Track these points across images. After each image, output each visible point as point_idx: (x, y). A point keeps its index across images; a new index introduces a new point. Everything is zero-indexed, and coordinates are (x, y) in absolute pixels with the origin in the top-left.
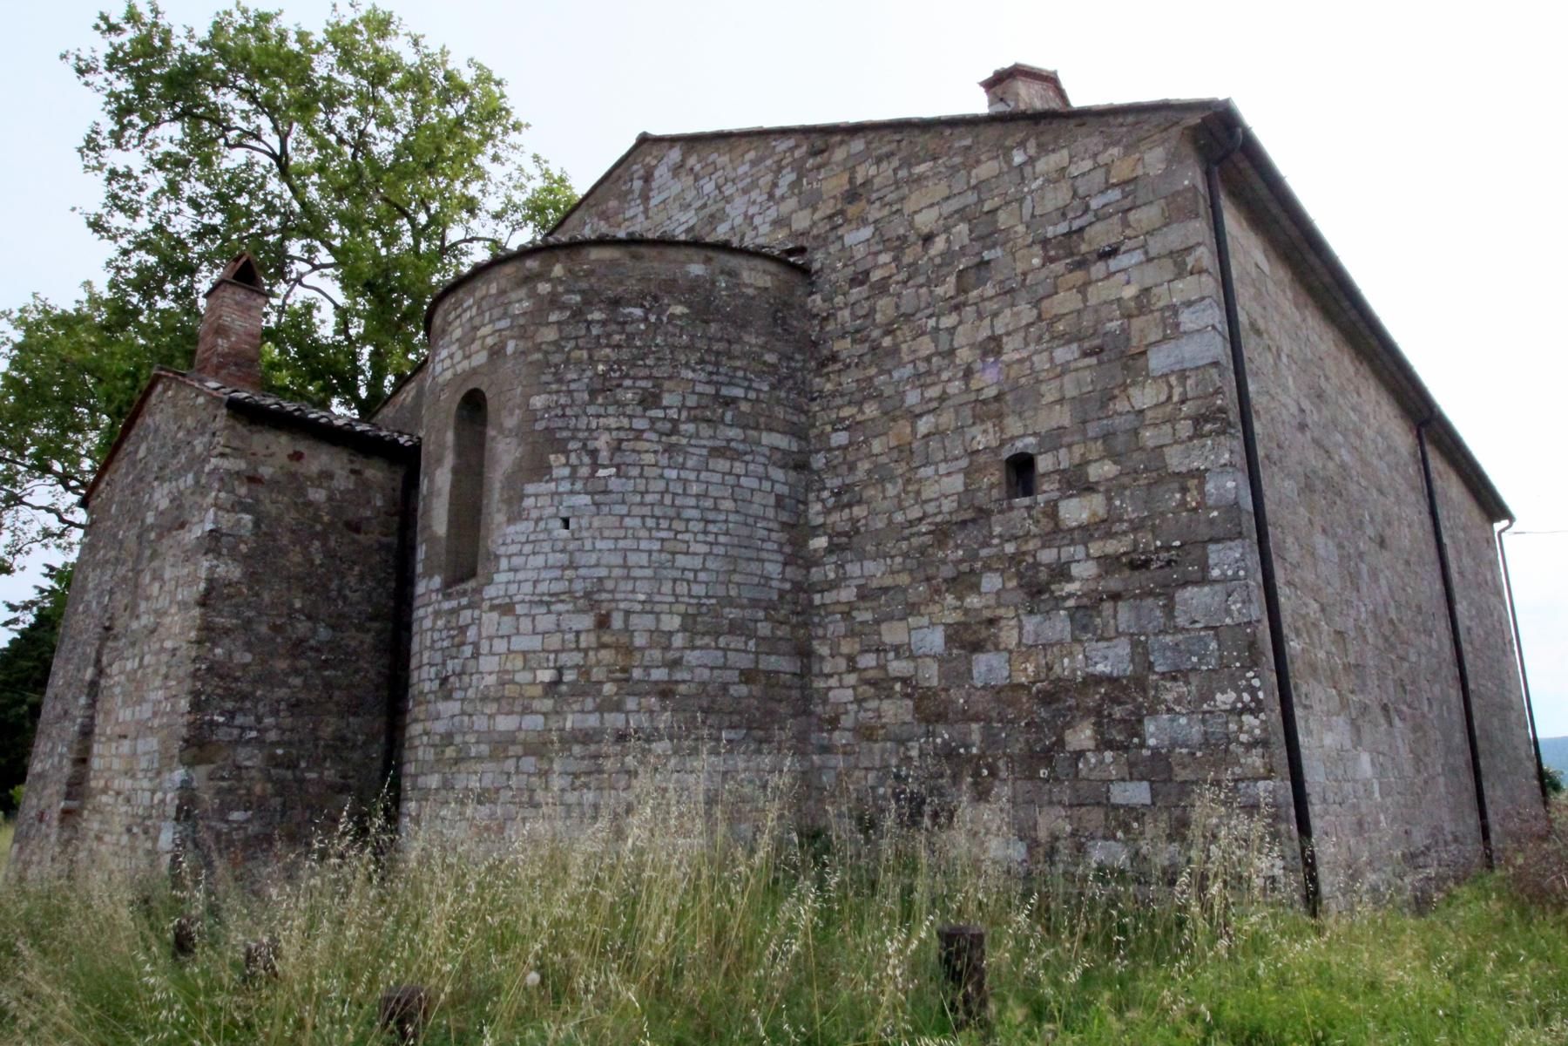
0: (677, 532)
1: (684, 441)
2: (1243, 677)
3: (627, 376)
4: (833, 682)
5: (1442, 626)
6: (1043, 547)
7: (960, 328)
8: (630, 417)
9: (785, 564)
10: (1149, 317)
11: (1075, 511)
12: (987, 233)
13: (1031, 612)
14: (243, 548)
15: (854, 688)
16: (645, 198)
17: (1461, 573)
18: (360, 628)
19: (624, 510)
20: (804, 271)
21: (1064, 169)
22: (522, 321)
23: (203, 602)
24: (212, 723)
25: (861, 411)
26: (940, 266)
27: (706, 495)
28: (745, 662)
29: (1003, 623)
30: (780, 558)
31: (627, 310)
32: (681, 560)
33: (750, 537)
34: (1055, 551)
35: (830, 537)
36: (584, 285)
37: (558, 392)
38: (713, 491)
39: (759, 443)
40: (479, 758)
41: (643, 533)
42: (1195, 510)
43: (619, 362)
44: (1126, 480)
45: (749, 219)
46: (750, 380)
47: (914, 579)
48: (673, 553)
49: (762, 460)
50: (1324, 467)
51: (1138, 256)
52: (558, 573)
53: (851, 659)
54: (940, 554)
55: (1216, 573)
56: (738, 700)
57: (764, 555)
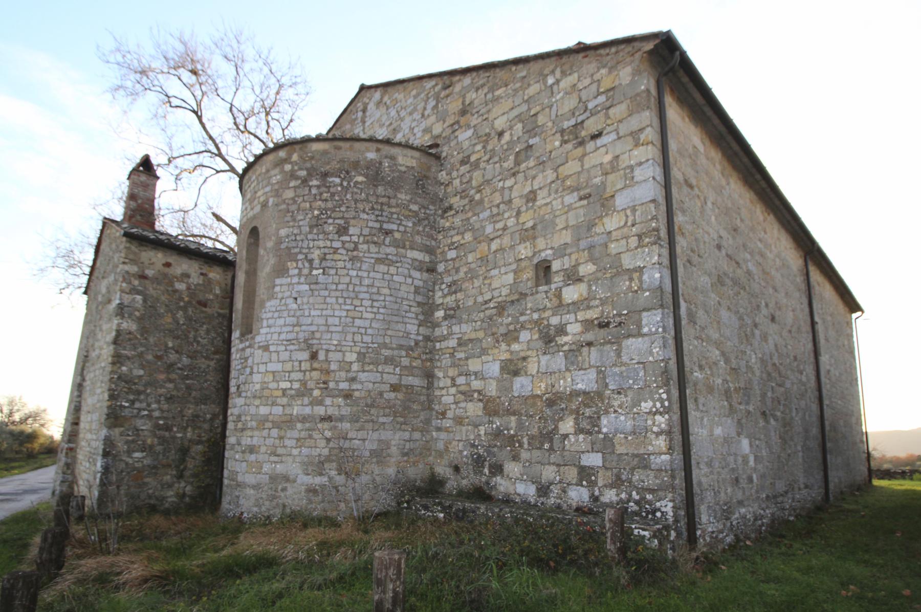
0: (356, 306)
1: (361, 255)
2: (657, 392)
3: (330, 217)
4: (444, 392)
5: (810, 370)
6: (553, 315)
7: (515, 187)
8: (331, 241)
9: (419, 326)
10: (617, 174)
11: (571, 294)
12: (532, 129)
13: (545, 353)
14: (137, 314)
15: (454, 395)
16: (364, 122)
17: (827, 340)
18: (207, 358)
19: (326, 293)
20: (437, 157)
21: (575, 85)
22: (276, 187)
23: (115, 342)
24: (122, 406)
25: (463, 238)
26: (506, 150)
27: (373, 286)
28: (394, 380)
29: (530, 359)
30: (416, 322)
31: (331, 180)
32: (358, 322)
33: (398, 310)
34: (559, 317)
35: (445, 311)
36: (308, 165)
37: (293, 227)
38: (377, 284)
39: (405, 257)
40: (252, 429)
41: (337, 307)
42: (636, 291)
43: (326, 209)
44: (599, 275)
45: (412, 129)
46: (401, 220)
47: (486, 335)
48: (353, 318)
49: (407, 266)
50: (734, 272)
51: (613, 136)
52: (290, 329)
53: (453, 379)
54: (500, 320)
55: (645, 330)
56: (388, 401)
57: (407, 320)
